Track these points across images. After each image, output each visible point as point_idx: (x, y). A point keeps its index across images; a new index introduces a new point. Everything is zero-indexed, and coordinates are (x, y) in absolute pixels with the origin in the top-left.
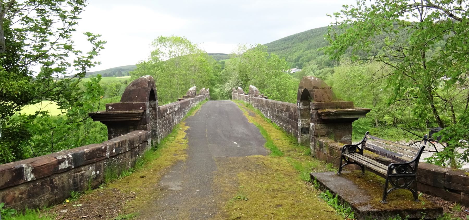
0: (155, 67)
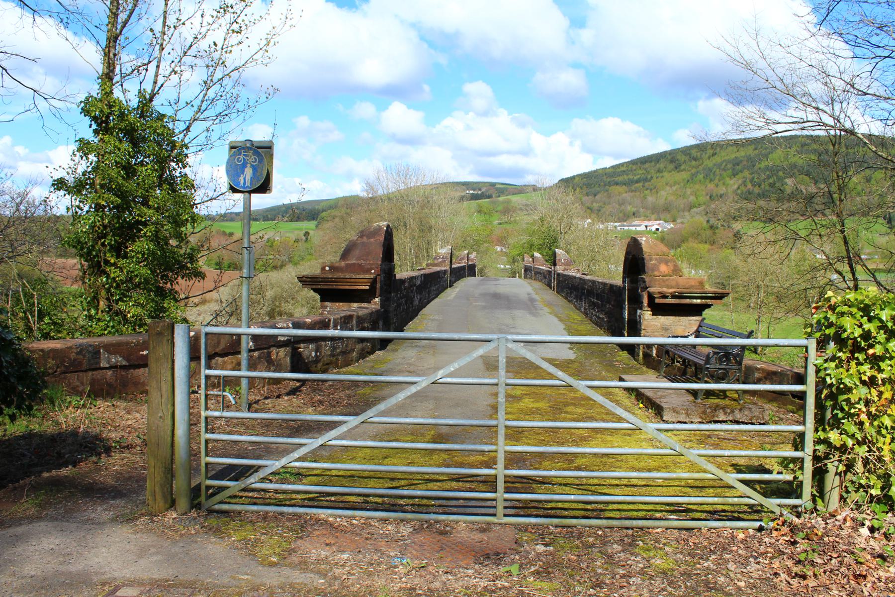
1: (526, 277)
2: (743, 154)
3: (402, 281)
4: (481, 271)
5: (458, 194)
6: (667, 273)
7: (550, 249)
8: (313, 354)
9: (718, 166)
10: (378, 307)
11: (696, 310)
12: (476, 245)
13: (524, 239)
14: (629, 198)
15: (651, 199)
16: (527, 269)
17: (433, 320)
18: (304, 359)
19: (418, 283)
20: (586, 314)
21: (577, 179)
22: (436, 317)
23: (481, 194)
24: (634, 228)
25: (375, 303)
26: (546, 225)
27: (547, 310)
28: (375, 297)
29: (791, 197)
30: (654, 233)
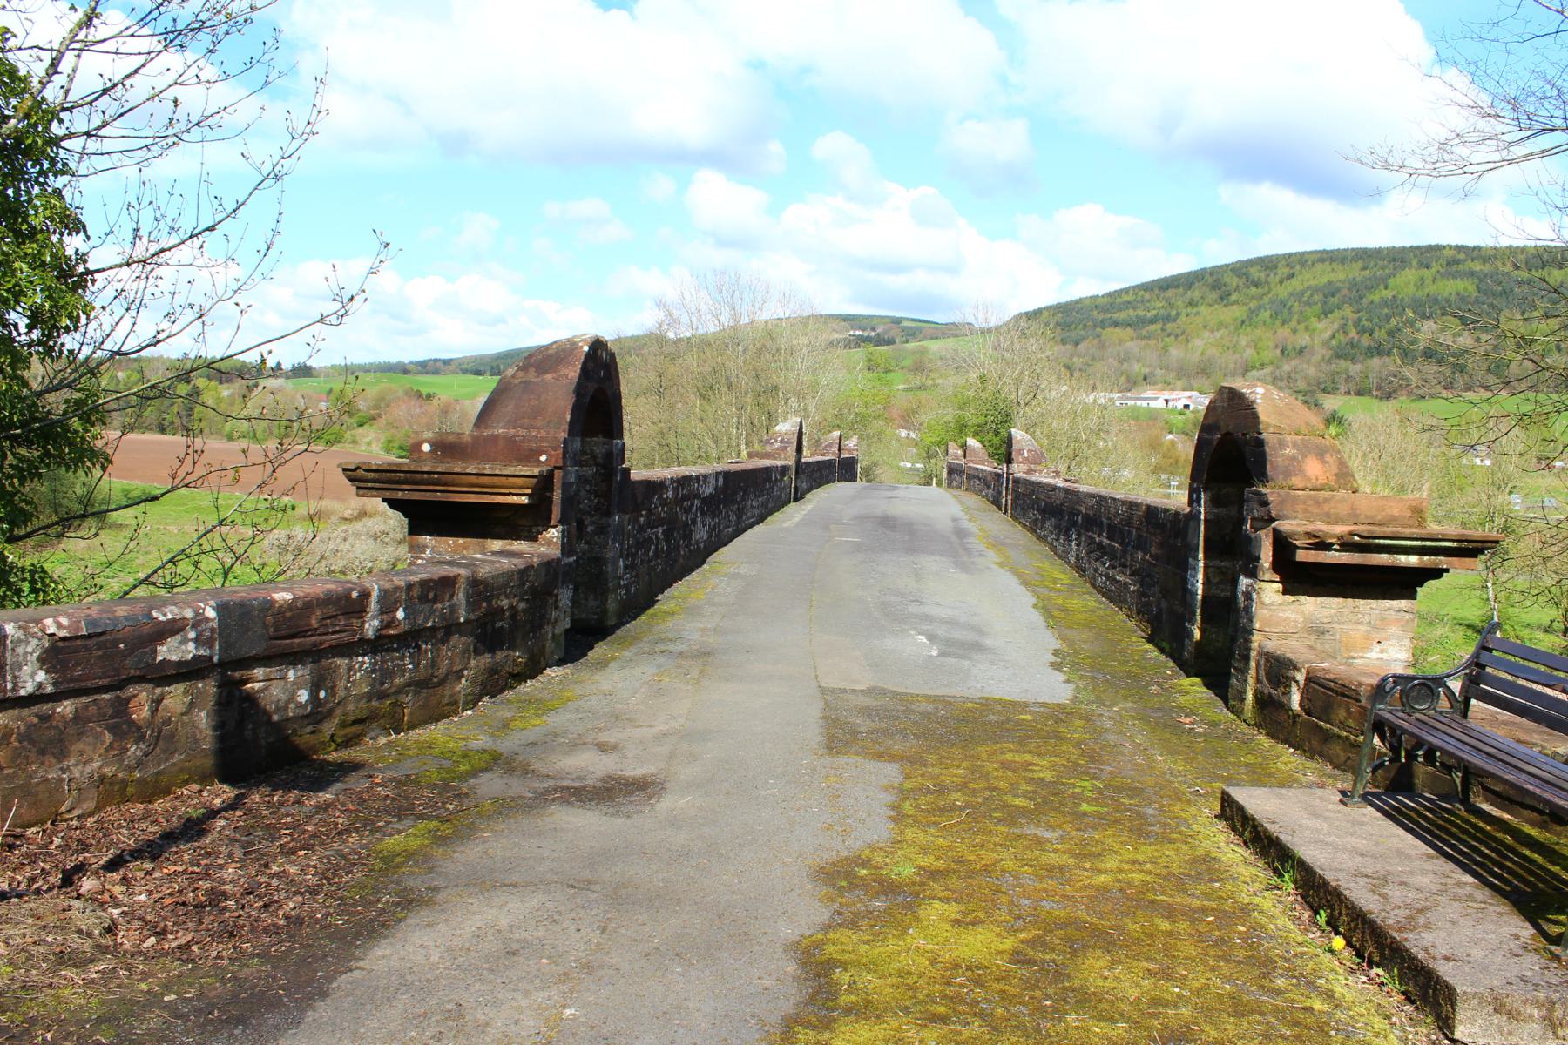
0: (1461, 318)
1: (950, 485)
2: (1342, 276)
3: (653, 487)
4: (867, 472)
5: (826, 336)
6: (1322, 481)
7: (997, 433)
8: (303, 696)
9: (1298, 296)
10: (556, 552)
11: (1401, 584)
12: (862, 422)
13: (950, 414)
14: (1136, 350)
15: (1175, 353)
16: (952, 470)
17: (735, 576)
18: (268, 715)
19: (708, 490)
20: (1081, 570)
21: (1046, 314)
22: (744, 570)
23: (876, 337)
24: (1144, 404)
25: (549, 542)
26: (990, 386)
27: (992, 555)
28: (547, 526)
29: (1429, 354)
30: (1181, 413)
